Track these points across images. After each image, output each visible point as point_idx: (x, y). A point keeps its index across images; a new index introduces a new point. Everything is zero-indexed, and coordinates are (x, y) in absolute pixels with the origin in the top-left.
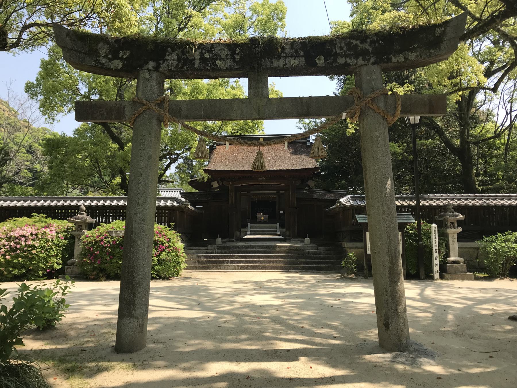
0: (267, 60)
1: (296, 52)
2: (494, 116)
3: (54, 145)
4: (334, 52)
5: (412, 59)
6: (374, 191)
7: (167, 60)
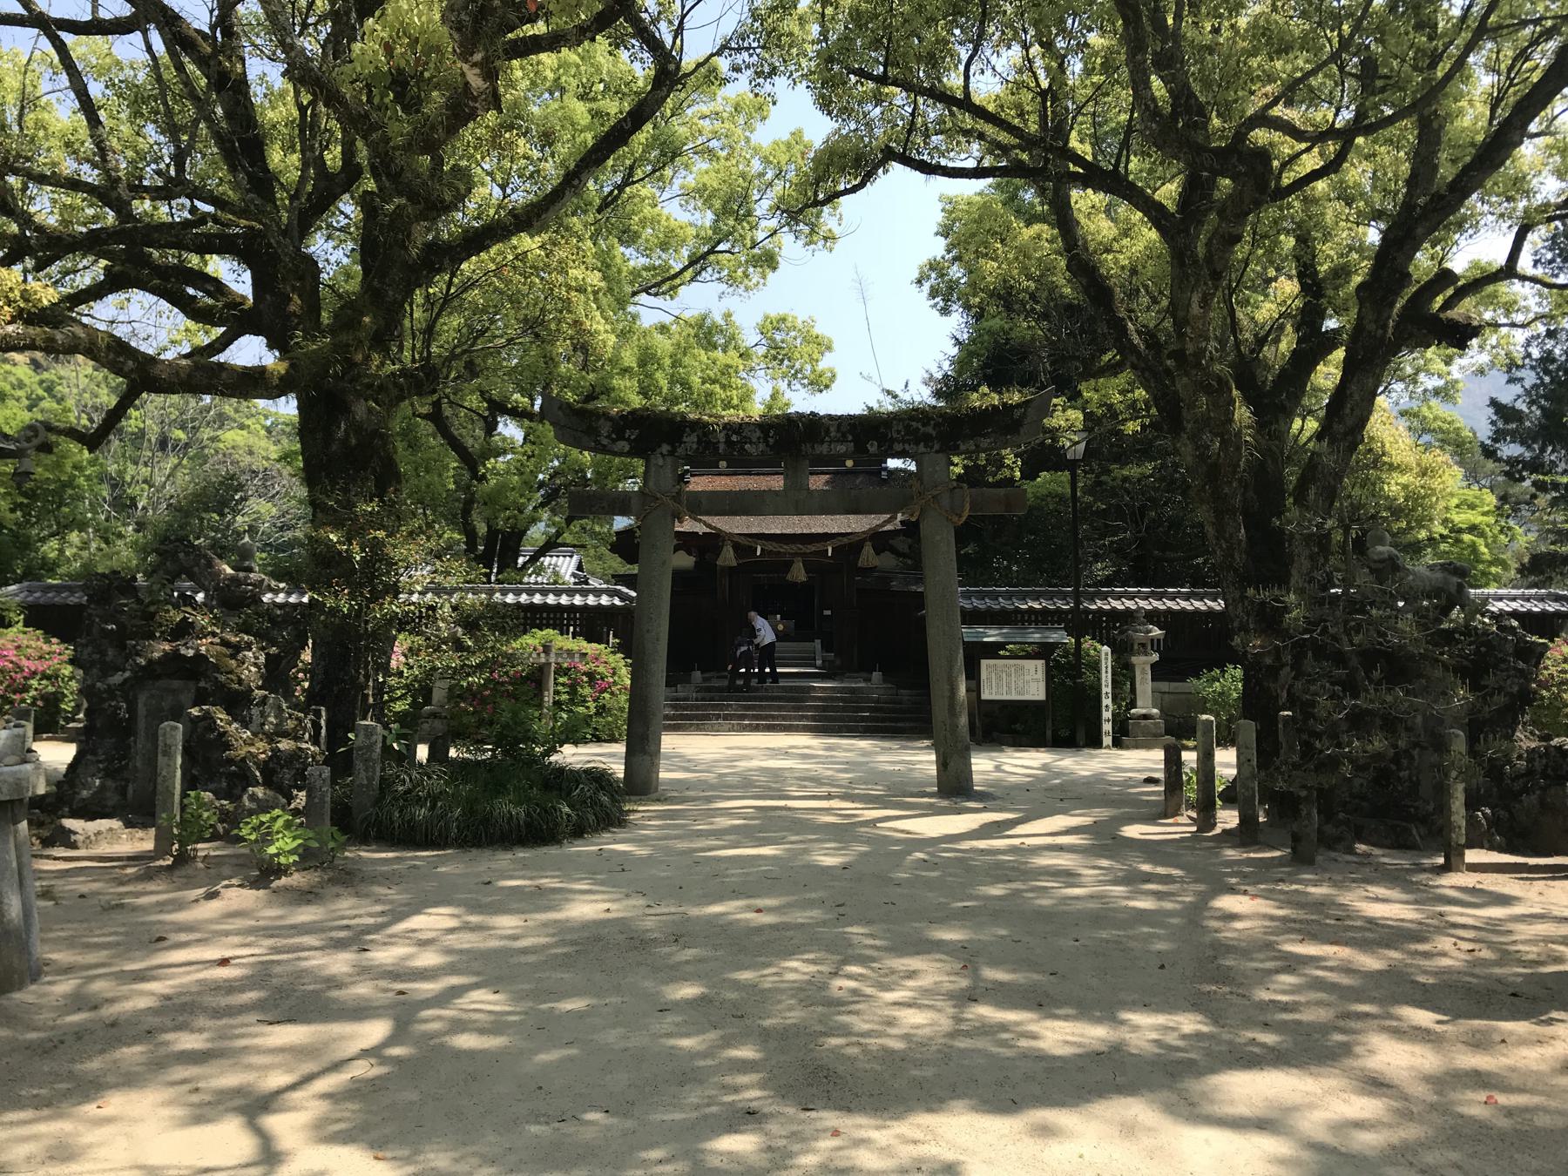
1: (844, 435)
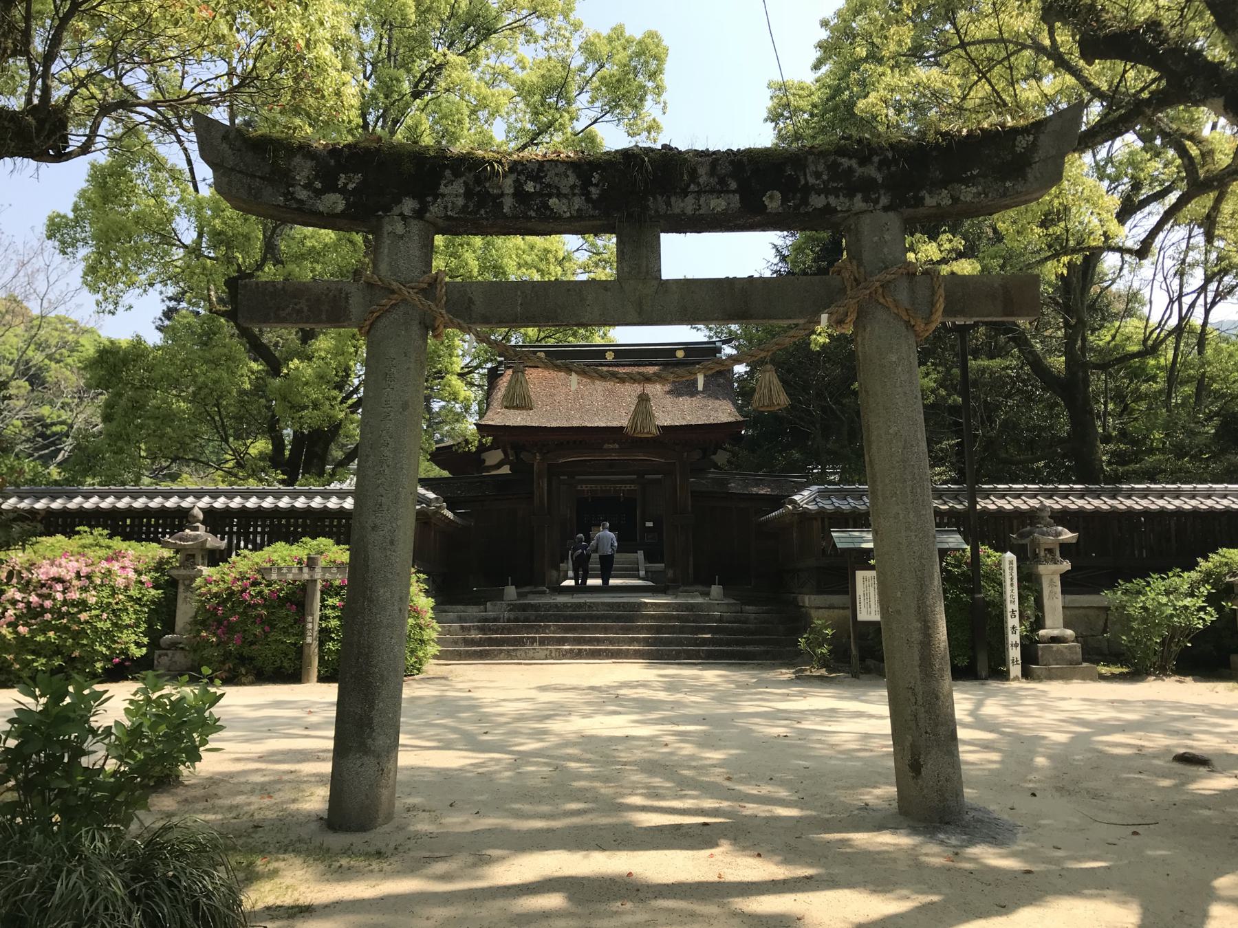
0: (659, 198)
1: (722, 181)
2: (1144, 305)
3: (112, 365)
4: (803, 182)
5: (968, 199)
6: (887, 481)
7: (443, 195)
